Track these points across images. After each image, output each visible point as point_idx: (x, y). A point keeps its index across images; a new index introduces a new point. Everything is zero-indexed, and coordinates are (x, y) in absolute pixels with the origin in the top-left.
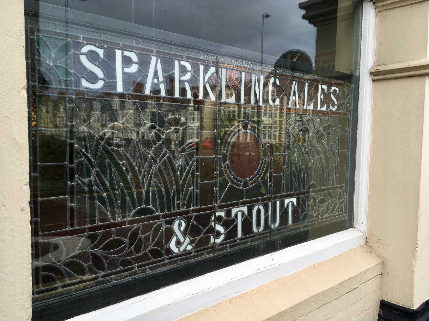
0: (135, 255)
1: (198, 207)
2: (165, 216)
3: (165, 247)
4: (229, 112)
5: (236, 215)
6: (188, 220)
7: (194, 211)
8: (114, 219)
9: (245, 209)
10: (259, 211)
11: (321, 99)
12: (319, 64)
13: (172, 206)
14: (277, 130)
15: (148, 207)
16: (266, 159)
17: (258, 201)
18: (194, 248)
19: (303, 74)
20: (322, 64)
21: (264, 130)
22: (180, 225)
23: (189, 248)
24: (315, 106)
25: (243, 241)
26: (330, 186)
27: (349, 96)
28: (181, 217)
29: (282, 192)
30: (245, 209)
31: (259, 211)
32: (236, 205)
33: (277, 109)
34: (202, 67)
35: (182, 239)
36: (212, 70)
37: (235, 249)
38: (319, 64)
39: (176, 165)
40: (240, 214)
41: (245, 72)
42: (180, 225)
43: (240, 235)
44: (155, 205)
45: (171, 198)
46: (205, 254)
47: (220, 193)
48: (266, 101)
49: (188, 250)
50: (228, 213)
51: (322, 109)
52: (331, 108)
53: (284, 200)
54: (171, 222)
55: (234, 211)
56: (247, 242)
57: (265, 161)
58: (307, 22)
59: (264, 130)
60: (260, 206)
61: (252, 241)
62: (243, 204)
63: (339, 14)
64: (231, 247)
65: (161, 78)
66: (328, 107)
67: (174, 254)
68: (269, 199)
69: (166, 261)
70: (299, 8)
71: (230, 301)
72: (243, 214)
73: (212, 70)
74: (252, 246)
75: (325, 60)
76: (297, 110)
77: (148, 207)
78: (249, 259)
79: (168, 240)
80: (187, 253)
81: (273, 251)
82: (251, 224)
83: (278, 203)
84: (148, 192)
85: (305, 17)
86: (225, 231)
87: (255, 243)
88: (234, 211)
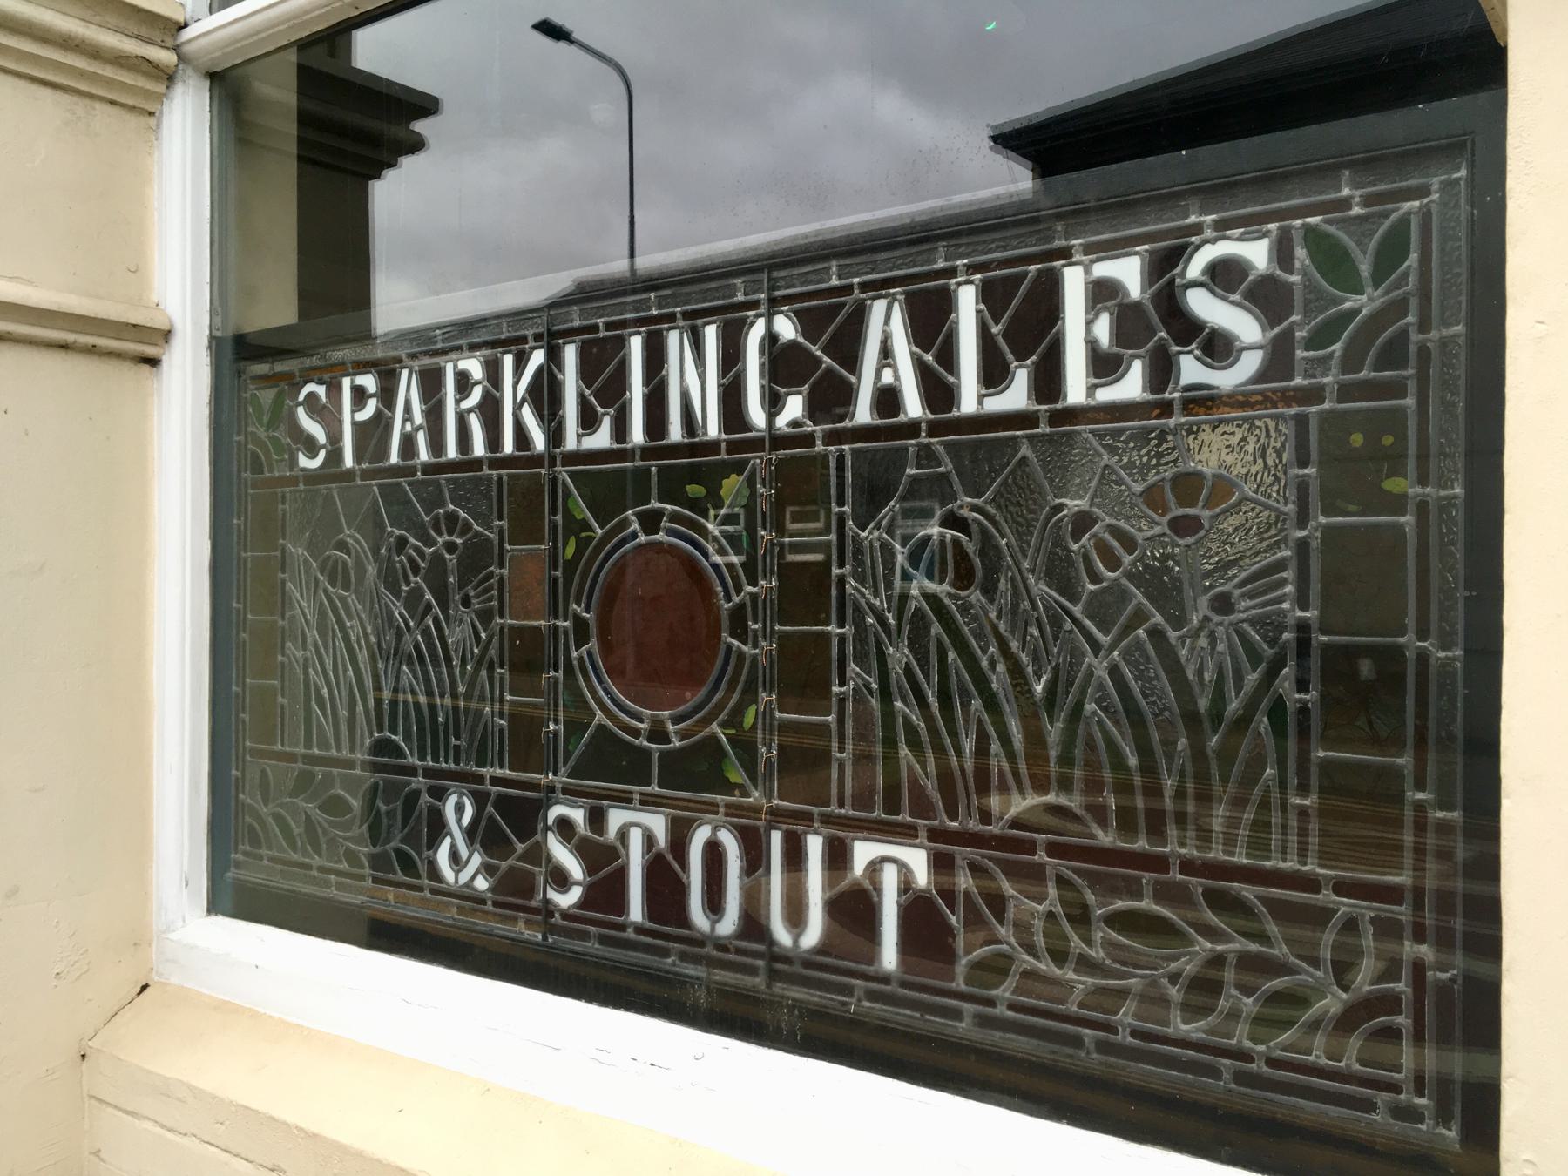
1: (843, 811)
2: (428, 773)
3: (426, 854)
5: (623, 835)
6: (480, 800)
7: (495, 781)
8: (339, 749)
9: (657, 823)
10: (714, 853)
13: (442, 753)
15: (393, 737)
16: (745, 649)
17: (712, 808)
18: (492, 889)
22: (460, 809)
23: (482, 884)
24: (1048, 381)
25: (649, 940)
26: (296, 746)
27: (1413, 259)
28: (465, 788)
30: (657, 823)
31: (714, 853)
32: (624, 800)
34: (508, 361)
35: (464, 852)
36: (538, 358)
37: (644, 959)
39: (450, 641)
40: (890, 877)
42: (460, 809)
43: (636, 911)
44: (407, 738)
45: (441, 728)
46: (521, 924)
47: (566, 741)
49: (475, 890)
50: (597, 819)
51: (999, 404)
53: (806, 833)
54: (439, 794)
55: (617, 818)
56: (665, 953)
57: (741, 655)
60: (723, 829)
61: (684, 957)
62: (648, 802)
65: (418, 419)
66: (1161, 372)
67: (444, 886)
68: (777, 816)
70: (401, 167)
71: (488, 1090)
72: (649, 839)
73: (538, 358)
74: (676, 974)
77: (393, 737)
78: (643, 1014)
79: (434, 843)
80: (468, 896)
81: (813, 1052)
82: (680, 890)
84: (394, 703)
86: (585, 878)
87: (690, 970)
88: (617, 818)
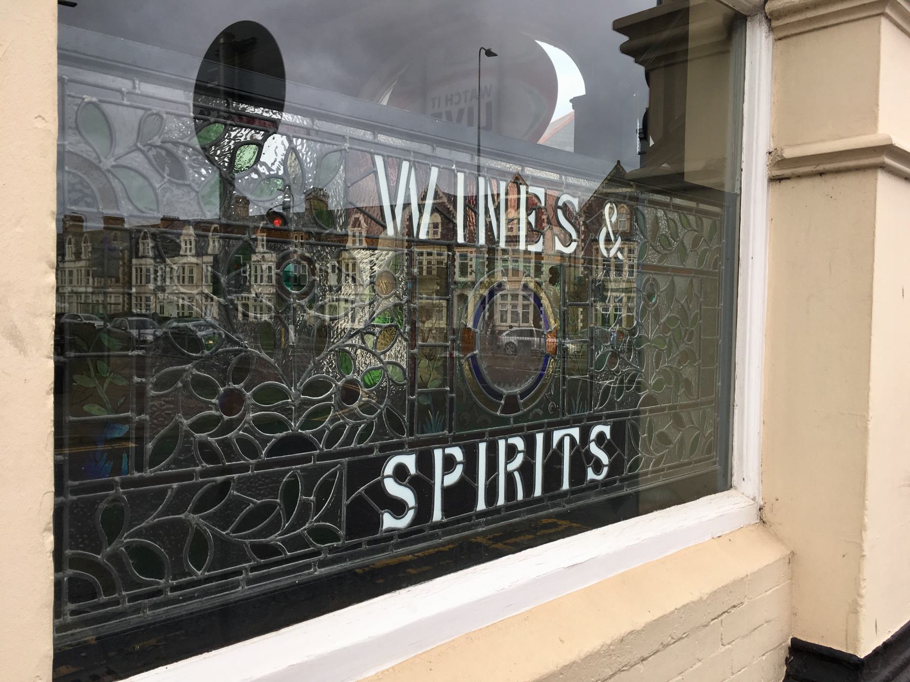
0: (255, 560)
4: (429, 263)
5: (561, 443)
9: (575, 432)
11: (529, 223)
12: (439, 107)
14: (506, 302)
19: (472, 155)
20: (446, 105)
21: (502, 302)
29: (561, 414)
30: (575, 432)
33: (84, 220)
38: (439, 107)
41: (409, 161)
48: (513, 240)
52: (559, 246)
58: (630, 60)
59: (502, 302)
63: (691, 45)
64: (359, 545)
69: (364, 547)
72: (572, 439)
75: (452, 95)
76: (572, 260)
83: (540, 437)
85: (625, 50)
